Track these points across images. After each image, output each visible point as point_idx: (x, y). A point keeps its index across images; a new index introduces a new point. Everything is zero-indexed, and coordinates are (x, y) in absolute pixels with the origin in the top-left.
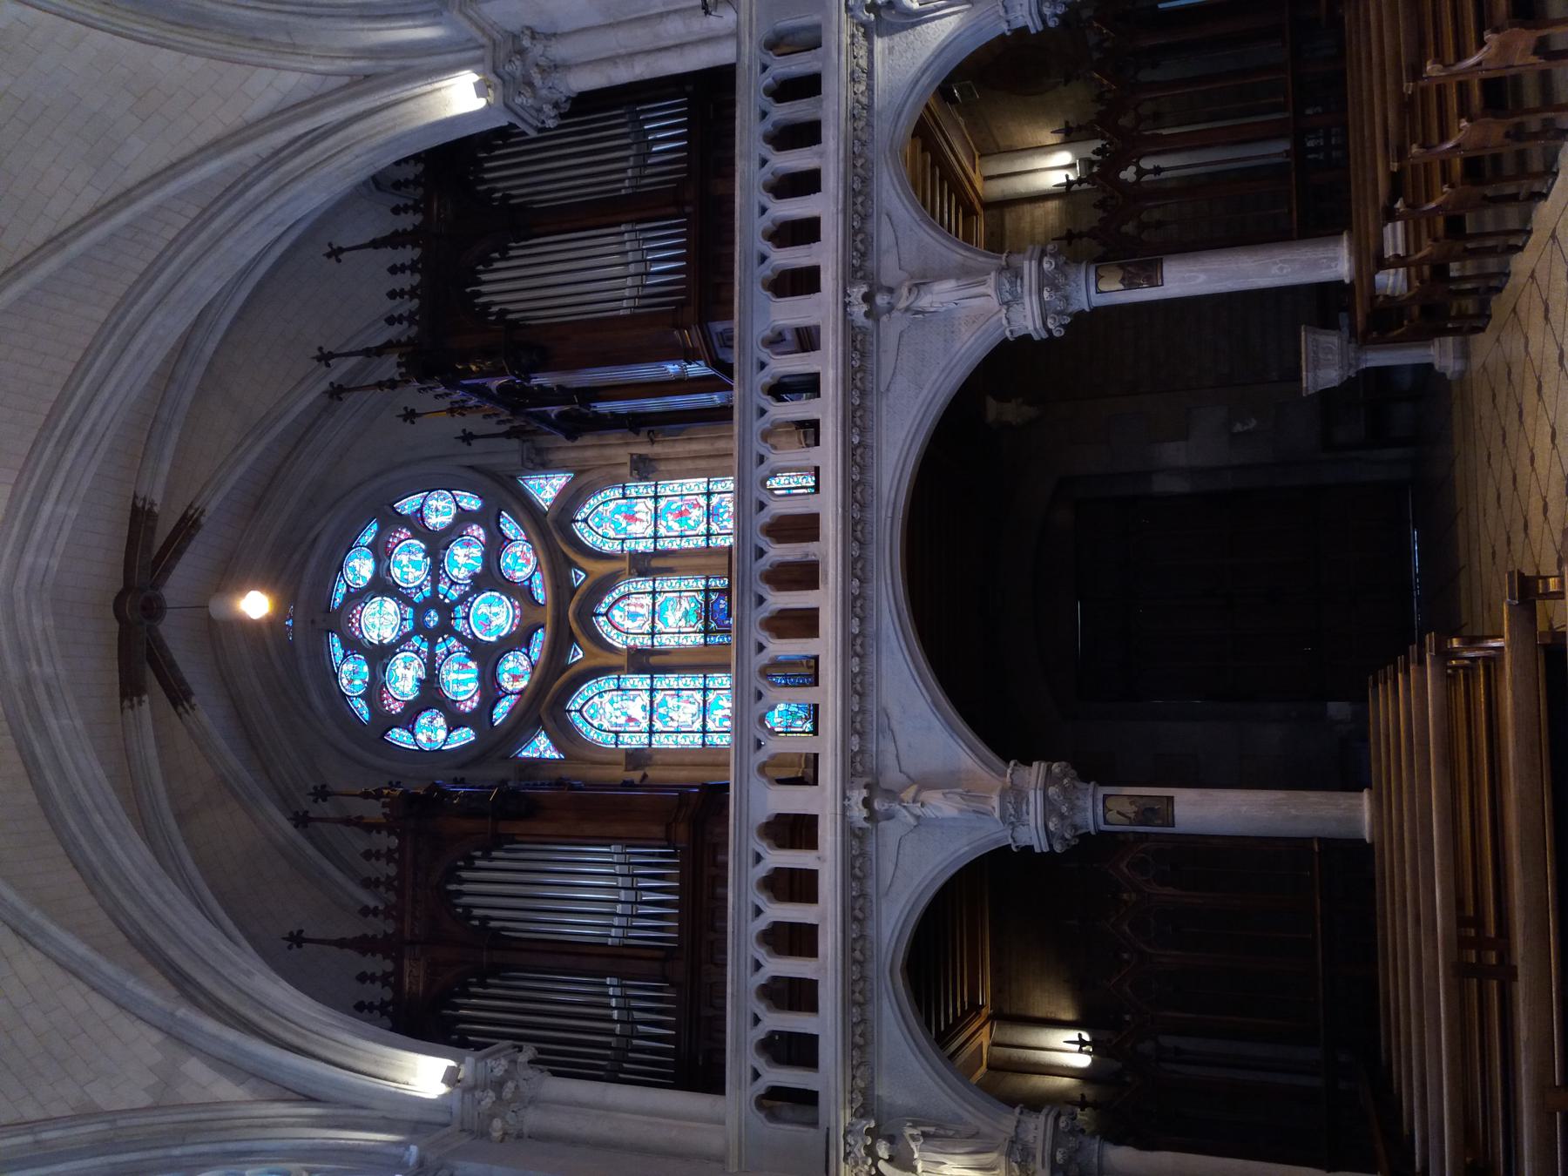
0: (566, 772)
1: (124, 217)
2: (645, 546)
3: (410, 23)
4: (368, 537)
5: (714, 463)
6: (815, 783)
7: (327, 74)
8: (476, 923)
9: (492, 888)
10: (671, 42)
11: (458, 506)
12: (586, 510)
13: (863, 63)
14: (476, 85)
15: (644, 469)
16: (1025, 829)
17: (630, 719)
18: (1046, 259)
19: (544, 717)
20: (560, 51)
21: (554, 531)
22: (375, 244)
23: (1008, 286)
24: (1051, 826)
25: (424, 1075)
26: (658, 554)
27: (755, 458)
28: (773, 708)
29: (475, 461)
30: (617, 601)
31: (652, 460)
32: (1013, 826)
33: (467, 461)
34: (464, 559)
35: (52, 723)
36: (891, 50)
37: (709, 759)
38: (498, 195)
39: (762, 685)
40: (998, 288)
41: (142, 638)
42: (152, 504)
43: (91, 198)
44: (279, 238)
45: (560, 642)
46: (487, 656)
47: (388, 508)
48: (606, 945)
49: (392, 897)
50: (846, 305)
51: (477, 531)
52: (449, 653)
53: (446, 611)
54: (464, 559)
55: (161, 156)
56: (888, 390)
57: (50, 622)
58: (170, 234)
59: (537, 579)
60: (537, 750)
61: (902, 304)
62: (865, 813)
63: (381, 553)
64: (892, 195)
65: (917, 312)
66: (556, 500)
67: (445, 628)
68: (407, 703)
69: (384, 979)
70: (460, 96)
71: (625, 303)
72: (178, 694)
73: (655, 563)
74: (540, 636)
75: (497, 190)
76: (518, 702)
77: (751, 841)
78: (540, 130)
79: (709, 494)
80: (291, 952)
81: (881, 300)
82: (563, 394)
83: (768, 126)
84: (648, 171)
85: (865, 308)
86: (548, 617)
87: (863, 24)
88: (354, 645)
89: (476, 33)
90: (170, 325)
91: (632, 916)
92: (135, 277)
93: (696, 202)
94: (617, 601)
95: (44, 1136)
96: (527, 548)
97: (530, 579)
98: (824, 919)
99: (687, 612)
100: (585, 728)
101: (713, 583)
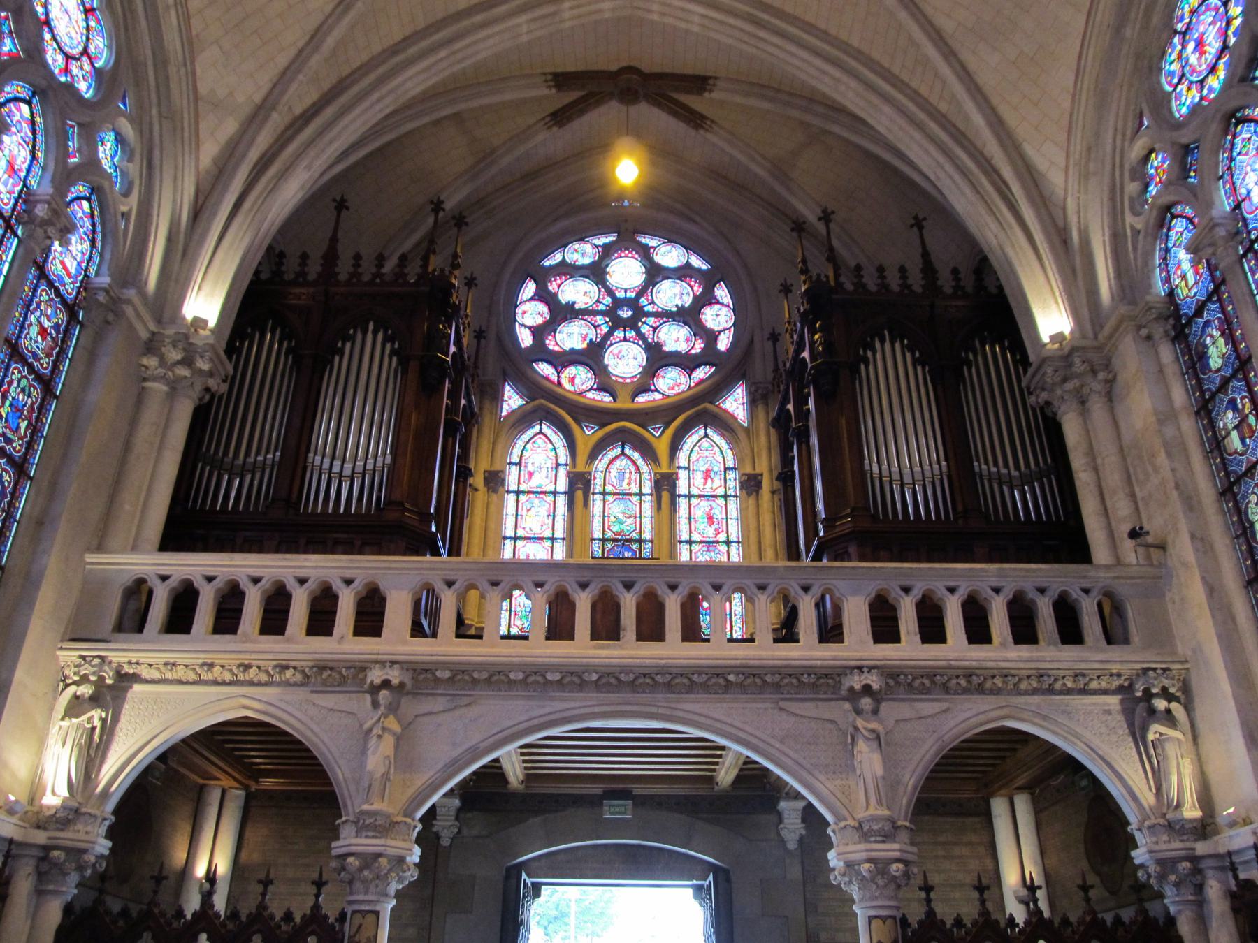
0: (487, 421)
1: (931, 51)
2: (682, 487)
3: (1112, 275)
4: (696, 262)
5: (754, 548)
6: (458, 636)
7: (1064, 209)
8: (339, 345)
9: (368, 359)
10: (1109, 504)
11: (720, 332)
12: (717, 438)
13: (1094, 685)
14: (1061, 335)
15: (751, 484)
16: (353, 833)
17: (531, 474)
18: (901, 866)
19: (536, 402)
20: (1097, 407)
21: (698, 411)
22: (925, 255)
23: (875, 827)
24: (351, 860)
25: (205, 304)
26: (674, 496)
27: (718, 581)
28: (528, 597)
29: (757, 346)
30: (634, 463)
31: (757, 492)
32: (356, 823)
33: (757, 339)
34: (675, 338)
35: (523, 18)
36: (1109, 712)
37: (490, 542)
38: (971, 357)
39: (550, 588)
40: (874, 819)
41: (596, 89)
42: (711, 91)
43: (947, 25)
44: (926, 177)
45: (599, 416)
46: (592, 356)
47: (719, 276)
48: (308, 451)
49: (366, 278)
50: (860, 668)
51: (699, 347)
52: (596, 327)
53: (632, 324)
54: (675, 338)
55: (986, 79)
56: (781, 709)
57: (607, 15)
58: (924, 90)
59: (657, 396)
60: (510, 398)
61: (860, 723)
62: (377, 681)
63: (683, 273)
64: (970, 716)
65: (853, 738)
66: (726, 411)
67: (617, 323)
68: (556, 295)
69: (302, 274)
70: (1052, 320)
71: (875, 465)
72: (560, 117)
73: (665, 496)
74: (607, 399)
75: (975, 356)
76: (553, 382)
77: (733, 582)
78: (1028, 388)
79: (728, 543)
80: (331, 200)
81: (866, 703)
82: (803, 415)
83: (1032, 594)
84: (996, 487)
85: (857, 687)
86: (624, 404)
87: (1131, 685)
88: (607, 252)
89: (1107, 330)
90: (850, 95)
91: (330, 472)
92: (887, 65)
93: (964, 527)
94: (634, 463)
95: (173, 13)
96: (683, 387)
97: (656, 390)
98: (289, 641)
99: (622, 523)
100: (526, 437)
101: (648, 546)
